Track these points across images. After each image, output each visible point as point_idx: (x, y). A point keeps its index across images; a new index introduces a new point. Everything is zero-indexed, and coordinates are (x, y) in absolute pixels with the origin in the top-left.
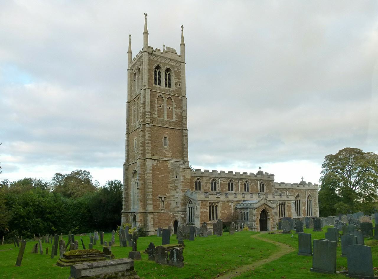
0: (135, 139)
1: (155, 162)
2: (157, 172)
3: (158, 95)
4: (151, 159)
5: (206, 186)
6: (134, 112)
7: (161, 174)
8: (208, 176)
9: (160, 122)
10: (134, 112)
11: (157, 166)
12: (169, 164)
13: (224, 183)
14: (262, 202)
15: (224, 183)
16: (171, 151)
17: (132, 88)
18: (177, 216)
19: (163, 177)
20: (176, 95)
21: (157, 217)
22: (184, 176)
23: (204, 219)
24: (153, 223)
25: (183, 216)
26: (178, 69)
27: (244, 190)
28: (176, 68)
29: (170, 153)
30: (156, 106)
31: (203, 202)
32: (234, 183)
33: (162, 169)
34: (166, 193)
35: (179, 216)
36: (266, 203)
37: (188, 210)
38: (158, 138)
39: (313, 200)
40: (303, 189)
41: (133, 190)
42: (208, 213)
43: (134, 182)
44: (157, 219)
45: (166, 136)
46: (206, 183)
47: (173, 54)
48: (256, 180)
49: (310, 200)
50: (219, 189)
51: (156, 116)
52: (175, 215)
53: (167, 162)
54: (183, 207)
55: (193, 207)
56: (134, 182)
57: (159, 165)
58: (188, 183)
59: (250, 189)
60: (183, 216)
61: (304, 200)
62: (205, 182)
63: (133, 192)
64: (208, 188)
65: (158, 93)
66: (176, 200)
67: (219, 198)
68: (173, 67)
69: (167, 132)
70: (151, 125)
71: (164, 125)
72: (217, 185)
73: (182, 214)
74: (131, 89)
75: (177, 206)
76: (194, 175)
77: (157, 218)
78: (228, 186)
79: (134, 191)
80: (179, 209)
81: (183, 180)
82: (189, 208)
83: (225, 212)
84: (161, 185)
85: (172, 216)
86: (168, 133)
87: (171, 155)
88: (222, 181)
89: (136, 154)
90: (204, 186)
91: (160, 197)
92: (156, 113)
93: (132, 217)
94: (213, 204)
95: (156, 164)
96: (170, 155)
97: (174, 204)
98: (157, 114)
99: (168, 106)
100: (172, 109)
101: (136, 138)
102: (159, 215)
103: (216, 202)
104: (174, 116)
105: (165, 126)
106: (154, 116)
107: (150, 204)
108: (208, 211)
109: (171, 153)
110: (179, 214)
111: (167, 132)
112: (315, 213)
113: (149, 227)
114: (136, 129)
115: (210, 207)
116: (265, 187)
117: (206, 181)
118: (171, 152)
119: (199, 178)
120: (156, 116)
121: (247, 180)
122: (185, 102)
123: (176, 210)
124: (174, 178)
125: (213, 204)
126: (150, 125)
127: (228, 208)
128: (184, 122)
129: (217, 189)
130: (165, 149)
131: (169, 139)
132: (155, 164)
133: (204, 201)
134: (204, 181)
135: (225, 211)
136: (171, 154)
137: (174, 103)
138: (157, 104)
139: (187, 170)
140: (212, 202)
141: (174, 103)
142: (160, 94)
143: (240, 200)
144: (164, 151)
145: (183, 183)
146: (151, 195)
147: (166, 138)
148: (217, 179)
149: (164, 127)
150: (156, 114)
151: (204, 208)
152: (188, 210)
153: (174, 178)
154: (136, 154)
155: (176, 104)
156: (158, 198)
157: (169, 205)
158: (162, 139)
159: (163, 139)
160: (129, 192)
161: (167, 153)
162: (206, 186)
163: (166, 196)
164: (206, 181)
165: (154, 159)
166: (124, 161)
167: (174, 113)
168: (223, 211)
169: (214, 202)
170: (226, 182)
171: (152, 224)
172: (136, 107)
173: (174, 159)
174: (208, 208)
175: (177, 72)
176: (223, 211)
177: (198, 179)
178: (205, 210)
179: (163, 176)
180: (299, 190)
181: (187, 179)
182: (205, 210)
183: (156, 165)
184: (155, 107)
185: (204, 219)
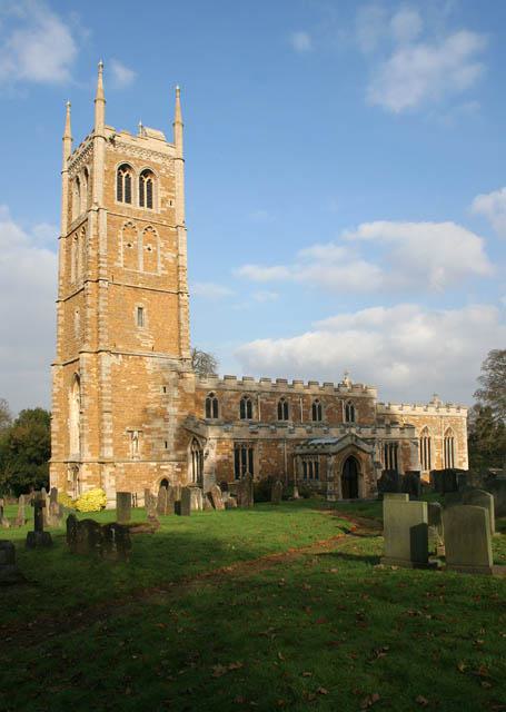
7: (132, 383)
14: (349, 441)
18: (166, 470)
20: (165, 223)
25: (179, 470)
26: (168, 171)
27: (311, 418)
30: (121, 244)
32: (290, 404)
39: (456, 437)
45: (141, 305)
57: (126, 365)
59: (324, 417)
60: (179, 470)
61: (437, 437)
68: (158, 167)
73: (178, 467)
92: (121, 258)
96: (150, 346)
100: (155, 252)
104: (160, 265)
105: (140, 285)
112: (460, 463)
116: (356, 413)
120: (122, 265)
129: (254, 415)
137: (159, 239)
141: (159, 239)
156: (125, 433)
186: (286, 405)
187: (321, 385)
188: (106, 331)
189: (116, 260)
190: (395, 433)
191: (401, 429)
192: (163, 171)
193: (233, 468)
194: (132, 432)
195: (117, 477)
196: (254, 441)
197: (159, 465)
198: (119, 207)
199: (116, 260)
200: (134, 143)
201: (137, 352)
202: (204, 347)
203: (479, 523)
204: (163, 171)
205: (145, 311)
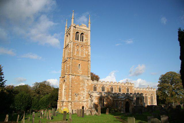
12: (81, 78)
20: (86, 45)
22: (88, 84)
45: (80, 64)
46: (99, 87)
57: (75, 78)
66: (83, 95)
72: (105, 89)
78: (110, 89)
96: (81, 73)
97: (82, 98)
104: (84, 55)
105: (80, 59)
116: (129, 90)
137: (84, 49)
148: (105, 85)
157: (80, 98)
167: (84, 53)
173: (84, 75)
186: (113, 88)
192: (86, 33)
201: (79, 75)
204: (86, 33)
205: (80, 65)
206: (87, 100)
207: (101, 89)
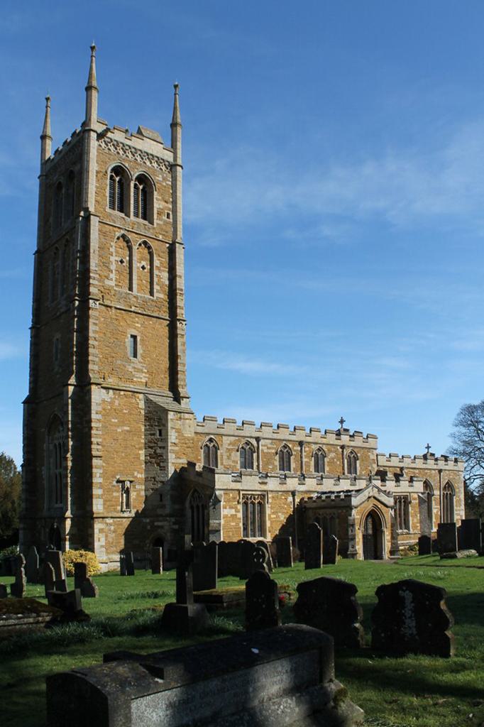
0: (55, 338)
1: (108, 393)
2: (113, 420)
3: (118, 234)
4: (99, 386)
5: (229, 458)
6: (54, 274)
7: (122, 423)
8: (232, 433)
9: (122, 298)
10: (54, 274)
11: (112, 403)
13: (270, 451)
15: (270, 451)
16: (146, 371)
17: (51, 220)
18: (162, 527)
19: (127, 431)
20: (161, 237)
21: (112, 528)
22: (178, 431)
23: (231, 534)
24: (104, 544)
25: (176, 527)
28: (160, 176)
29: (144, 375)
30: (113, 259)
31: (228, 492)
33: (125, 411)
34: (135, 471)
35: (166, 528)
36: (377, 495)
37: (189, 513)
38: (114, 336)
40: (434, 470)
41: (49, 463)
42: (240, 519)
43: (51, 445)
44: (114, 535)
47: (155, 143)
48: (339, 447)
49: (200, 505)
50: (259, 462)
51: (112, 283)
52: (156, 524)
53: (137, 395)
54: (177, 507)
55: (203, 505)
56: (51, 445)
57: (117, 402)
58: (188, 447)
60: (176, 527)
62: (227, 449)
63: (50, 469)
64: (234, 461)
65: (116, 229)
67: (266, 483)
69: (137, 325)
70: (100, 304)
71: (143, 345)
73: (174, 523)
74: (48, 221)
75: (161, 503)
76: (200, 429)
77: (114, 532)
78: (277, 457)
79: (51, 466)
80: (168, 511)
81: (177, 441)
82: (192, 507)
83: (278, 517)
84: (122, 452)
85: (149, 527)
86: (139, 326)
87: (147, 379)
88: (265, 446)
89: (58, 376)
90: (225, 457)
91: (118, 481)
92: (113, 276)
93: (47, 530)
94: (251, 499)
95: (111, 398)
96: (144, 380)
98: (114, 279)
99: (140, 262)
101: (58, 336)
102: (118, 525)
103: (259, 495)
105: (133, 309)
106: (107, 282)
107: (99, 497)
108: (240, 515)
109: (147, 375)
110: (165, 523)
111: (137, 325)
113: (220, 468)
114: (58, 314)
115: (246, 504)
117: (229, 445)
118: (145, 373)
119: (212, 436)
120: (112, 283)
121: (321, 446)
122: (164, 688)
123: (159, 511)
124: (154, 434)
125: (251, 499)
126: (97, 303)
127: (285, 509)
128: (174, 301)
130: (132, 364)
131: (142, 340)
132: (109, 400)
133: (232, 490)
134: (224, 446)
135: (280, 514)
136: (145, 377)
138: (114, 254)
139: (187, 416)
140: (249, 495)
142: (123, 232)
143: (311, 489)
144: (130, 370)
145: (177, 448)
146: (98, 475)
147: (134, 337)
149: (131, 311)
150: (112, 280)
151: (231, 508)
152: (189, 513)
153: (154, 434)
154: (58, 376)
155: (159, 260)
156: (115, 483)
158: (126, 340)
159: (129, 341)
160: (38, 469)
161: (138, 375)
162: (229, 458)
163: (136, 477)
164: (229, 445)
165: (107, 386)
166: (25, 392)
168: (275, 516)
169: (254, 493)
170: (273, 448)
171: (102, 546)
172: (59, 262)
174: (240, 507)
175: (163, 186)
176: (275, 516)
177: (211, 440)
178: (233, 512)
179: (128, 428)
180: (426, 471)
181: (185, 438)
182: (233, 512)
183: (110, 403)
184: (110, 262)
185: (231, 534)
187: (413, 458)
188: (97, 359)
189: (107, 277)
190: (358, 442)
191: (351, 436)
193: (241, 525)
194: (123, 482)
195: (106, 536)
196: (263, 496)
197: (152, 522)
198: (111, 215)
199: (107, 277)
200: (128, 142)
201: (132, 387)
202: (422, 454)
203: (145, 293)
206: (177, 507)
207: (237, 457)
